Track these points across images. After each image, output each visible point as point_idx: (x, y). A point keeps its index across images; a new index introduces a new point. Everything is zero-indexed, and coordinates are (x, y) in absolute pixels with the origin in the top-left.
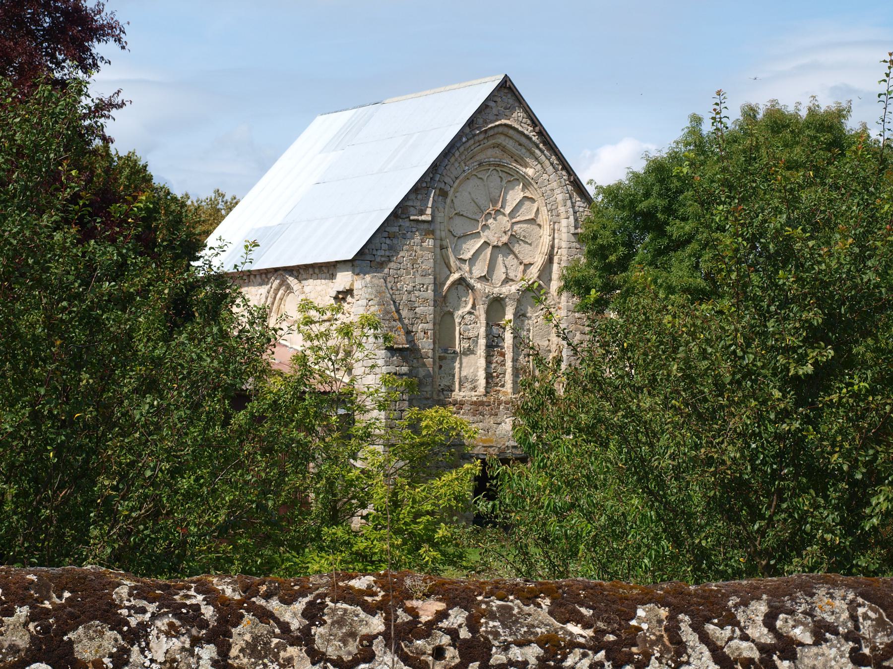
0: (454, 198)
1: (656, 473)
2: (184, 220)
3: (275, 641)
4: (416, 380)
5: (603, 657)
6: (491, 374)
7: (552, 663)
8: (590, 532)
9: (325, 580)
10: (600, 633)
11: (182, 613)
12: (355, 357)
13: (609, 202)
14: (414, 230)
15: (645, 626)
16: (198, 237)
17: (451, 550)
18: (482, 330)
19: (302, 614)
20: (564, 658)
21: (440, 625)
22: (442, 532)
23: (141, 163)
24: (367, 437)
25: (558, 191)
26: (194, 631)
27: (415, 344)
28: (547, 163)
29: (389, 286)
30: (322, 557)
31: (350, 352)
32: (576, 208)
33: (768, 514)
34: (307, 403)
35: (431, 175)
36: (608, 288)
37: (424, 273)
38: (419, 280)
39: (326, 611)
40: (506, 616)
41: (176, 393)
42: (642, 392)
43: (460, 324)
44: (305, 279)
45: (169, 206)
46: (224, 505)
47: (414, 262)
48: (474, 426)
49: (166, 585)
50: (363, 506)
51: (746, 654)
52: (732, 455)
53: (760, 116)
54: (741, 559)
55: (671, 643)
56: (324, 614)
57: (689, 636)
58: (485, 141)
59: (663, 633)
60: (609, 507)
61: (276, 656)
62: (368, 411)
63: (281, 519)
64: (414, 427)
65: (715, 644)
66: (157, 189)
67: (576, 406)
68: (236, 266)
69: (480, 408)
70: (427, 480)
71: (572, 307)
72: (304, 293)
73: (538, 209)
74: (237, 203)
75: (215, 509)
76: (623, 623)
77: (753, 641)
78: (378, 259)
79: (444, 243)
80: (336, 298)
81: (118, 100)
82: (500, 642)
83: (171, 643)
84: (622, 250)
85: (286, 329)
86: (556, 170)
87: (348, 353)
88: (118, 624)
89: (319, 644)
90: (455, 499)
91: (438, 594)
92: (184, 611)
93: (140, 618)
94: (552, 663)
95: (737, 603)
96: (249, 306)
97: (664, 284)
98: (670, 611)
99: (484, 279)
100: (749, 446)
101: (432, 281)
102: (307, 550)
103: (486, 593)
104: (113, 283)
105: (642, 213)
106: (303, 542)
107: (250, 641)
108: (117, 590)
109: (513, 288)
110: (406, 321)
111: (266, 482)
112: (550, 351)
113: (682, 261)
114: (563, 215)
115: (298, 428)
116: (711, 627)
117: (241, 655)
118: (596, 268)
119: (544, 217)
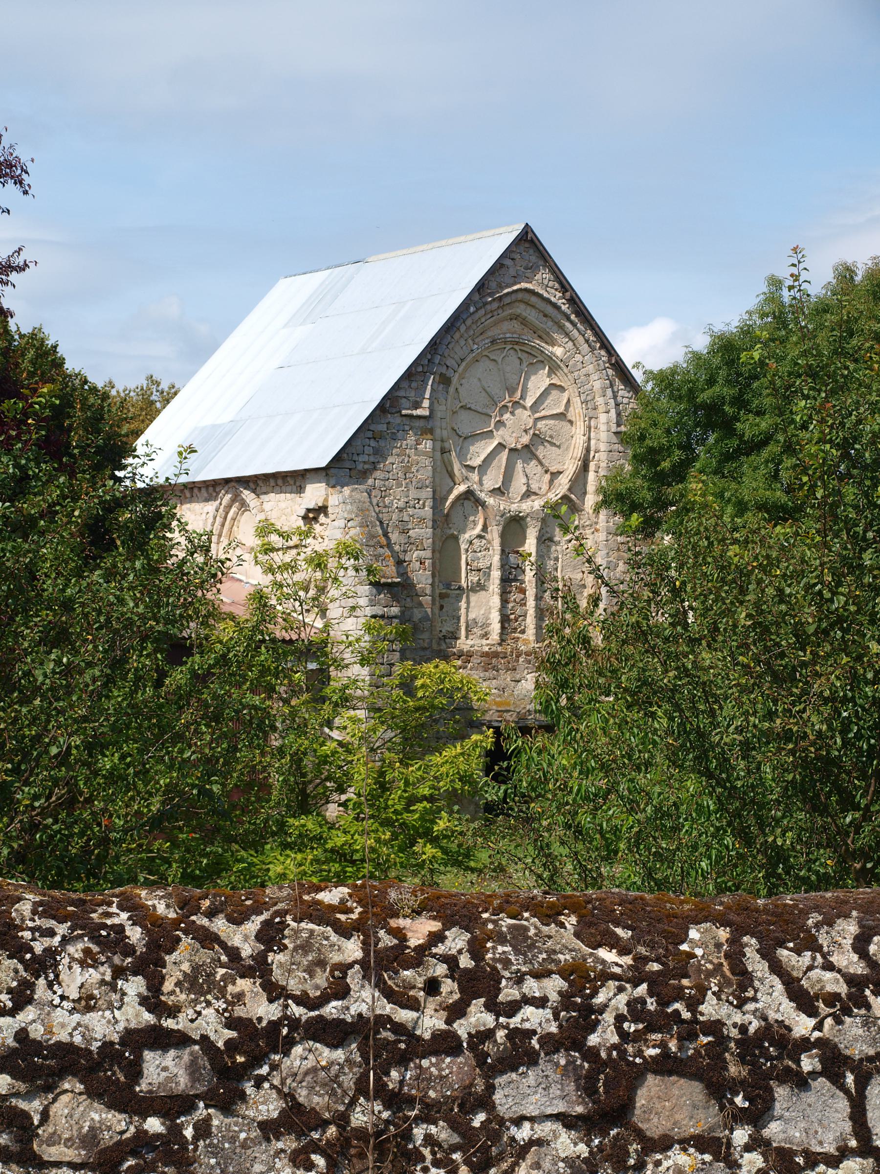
0: (458, 386)
1: (718, 750)
2: (106, 416)
3: (221, 971)
4: (408, 626)
5: (645, 992)
6: (508, 616)
7: (579, 1000)
8: (632, 827)
9: (286, 893)
10: (641, 960)
11: (101, 935)
12: (329, 595)
13: (661, 391)
14: (407, 428)
15: (699, 952)
16: (124, 439)
17: (454, 847)
18: (496, 559)
19: (256, 937)
20: (595, 993)
21: (434, 950)
22: (441, 825)
23: (50, 342)
24: (345, 701)
25: (594, 377)
26: (117, 960)
27: (408, 578)
28: (581, 339)
29: (375, 501)
30: (288, 856)
31: (324, 588)
32: (619, 399)
33: (863, 802)
34: (263, 658)
35: (429, 357)
36: (661, 503)
37: (420, 485)
38: (413, 494)
39: (286, 932)
40: (518, 940)
41: (90, 647)
42: (700, 644)
43: (467, 551)
44: (265, 493)
45: (86, 399)
46: (158, 790)
47: (407, 470)
48: (485, 684)
49: (80, 900)
50: (341, 790)
51: (830, 988)
52: (817, 727)
53: (858, 279)
54: (829, 862)
55: (733, 974)
56: (284, 937)
57: (756, 964)
58: (500, 311)
59: (723, 960)
60: (656, 795)
61: (223, 991)
62: (347, 666)
63: (234, 807)
64: (408, 687)
65: (789, 975)
66: (70, 376)
67: (617, 659)
68: (167, 479)
69: (494, 660)
70: (424, 755)
71: (613, 529)
72: (263, 511)
73: (569, 401)
74: (176, 394)
75: (146, 796)
76: (670, 947)
77: (839, 971)
78: (360, 467)
79: (446, 445)
80: (305, 518)
81: (19, 261)
82: (511, 973)
83: (87, 975)
84: (678, 455)
85: (235, 559)
86: (593, 349)
87: (322, 590)
88: (18, 950)
89: (277, 975)
90: (460, 780)
91: (431, 910)
92: (104, 933)
93: (47, 942)
94: (579, 1000)
95: (818, 922)
96: (187, 531)
97: (734, 499)
98: (732, 932)
99: (498, 492)
100: (840, 714)
101: (430, 495)
102: (268, 847)
103: (494, 909)
104: (7, 504)
105: (704, 406)
106: (262, 837)
107: (189, 972)
108: (17, 906)
109: (536, 504)
110: (397, 548)
111: (209, 761)
112: (584, 586)
113: (756, 468)
114: (602, 408)
115: (254, 692)
116: (785, 952)
117: (178, 990)
118: (644, 477)
119: (577, 411)
